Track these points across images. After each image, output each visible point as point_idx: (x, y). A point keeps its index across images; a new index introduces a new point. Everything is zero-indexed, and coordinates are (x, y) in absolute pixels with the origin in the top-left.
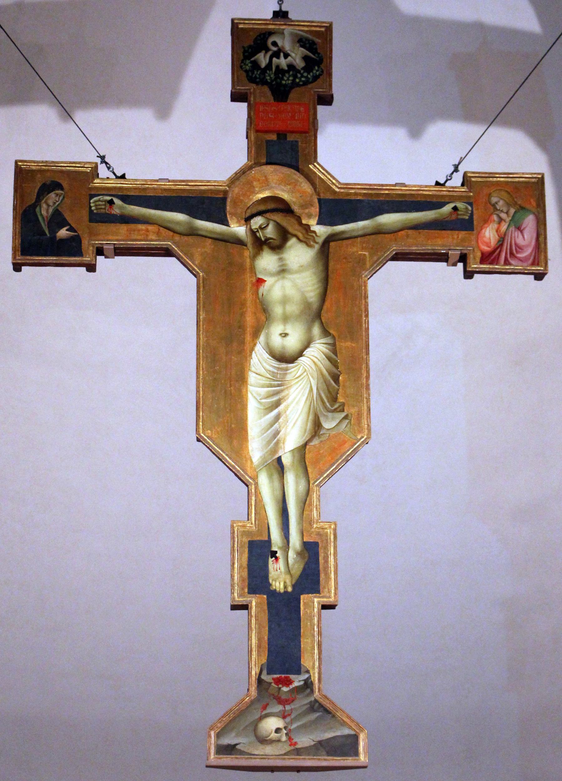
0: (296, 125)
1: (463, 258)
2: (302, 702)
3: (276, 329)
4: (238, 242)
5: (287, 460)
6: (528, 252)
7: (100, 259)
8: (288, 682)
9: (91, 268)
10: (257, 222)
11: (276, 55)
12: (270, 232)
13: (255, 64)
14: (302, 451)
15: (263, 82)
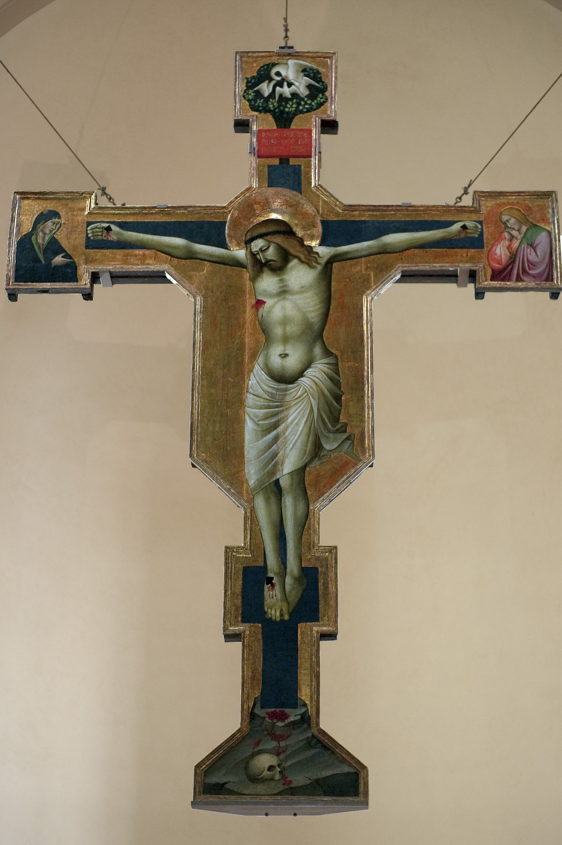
1: (473, 276)
3: (276, 350)
4: (237, 264)
5: (285, 483)
8: (286, 716)
10: (258, 244)
11: (280, 84)
12: (271, 253)
13: (259, 94)
15: (266, 110)
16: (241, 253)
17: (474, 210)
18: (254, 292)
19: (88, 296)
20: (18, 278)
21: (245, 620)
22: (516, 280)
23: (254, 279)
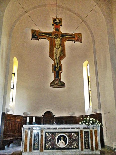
0: (58, 27)
1: (74, 41)
2: (59, 81)
3: (56, 46)
4: (53, 38)
5: (57, 58)
6: (80, 40)
7: (40, 39)
8: (58, 79)
9: (39, 40)
10: (55, 36)
11: (56, 21)
12: (56, 37)
13: (54, 22)
14: (59, 57)
15: (55, 23)
16: (53, 37)
17: (74, 34)
18: (54, 41)
19: (39, 40)
20: (32, 38)
21: (54, 70)
22: (77, 41)
23: (55, 39)
